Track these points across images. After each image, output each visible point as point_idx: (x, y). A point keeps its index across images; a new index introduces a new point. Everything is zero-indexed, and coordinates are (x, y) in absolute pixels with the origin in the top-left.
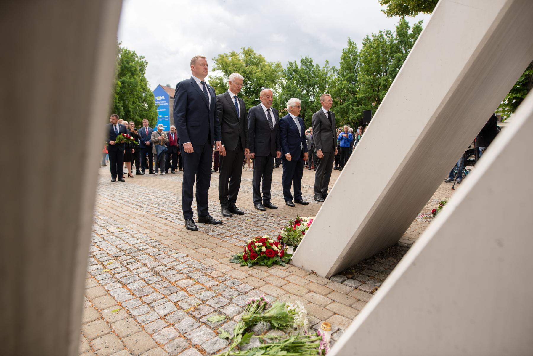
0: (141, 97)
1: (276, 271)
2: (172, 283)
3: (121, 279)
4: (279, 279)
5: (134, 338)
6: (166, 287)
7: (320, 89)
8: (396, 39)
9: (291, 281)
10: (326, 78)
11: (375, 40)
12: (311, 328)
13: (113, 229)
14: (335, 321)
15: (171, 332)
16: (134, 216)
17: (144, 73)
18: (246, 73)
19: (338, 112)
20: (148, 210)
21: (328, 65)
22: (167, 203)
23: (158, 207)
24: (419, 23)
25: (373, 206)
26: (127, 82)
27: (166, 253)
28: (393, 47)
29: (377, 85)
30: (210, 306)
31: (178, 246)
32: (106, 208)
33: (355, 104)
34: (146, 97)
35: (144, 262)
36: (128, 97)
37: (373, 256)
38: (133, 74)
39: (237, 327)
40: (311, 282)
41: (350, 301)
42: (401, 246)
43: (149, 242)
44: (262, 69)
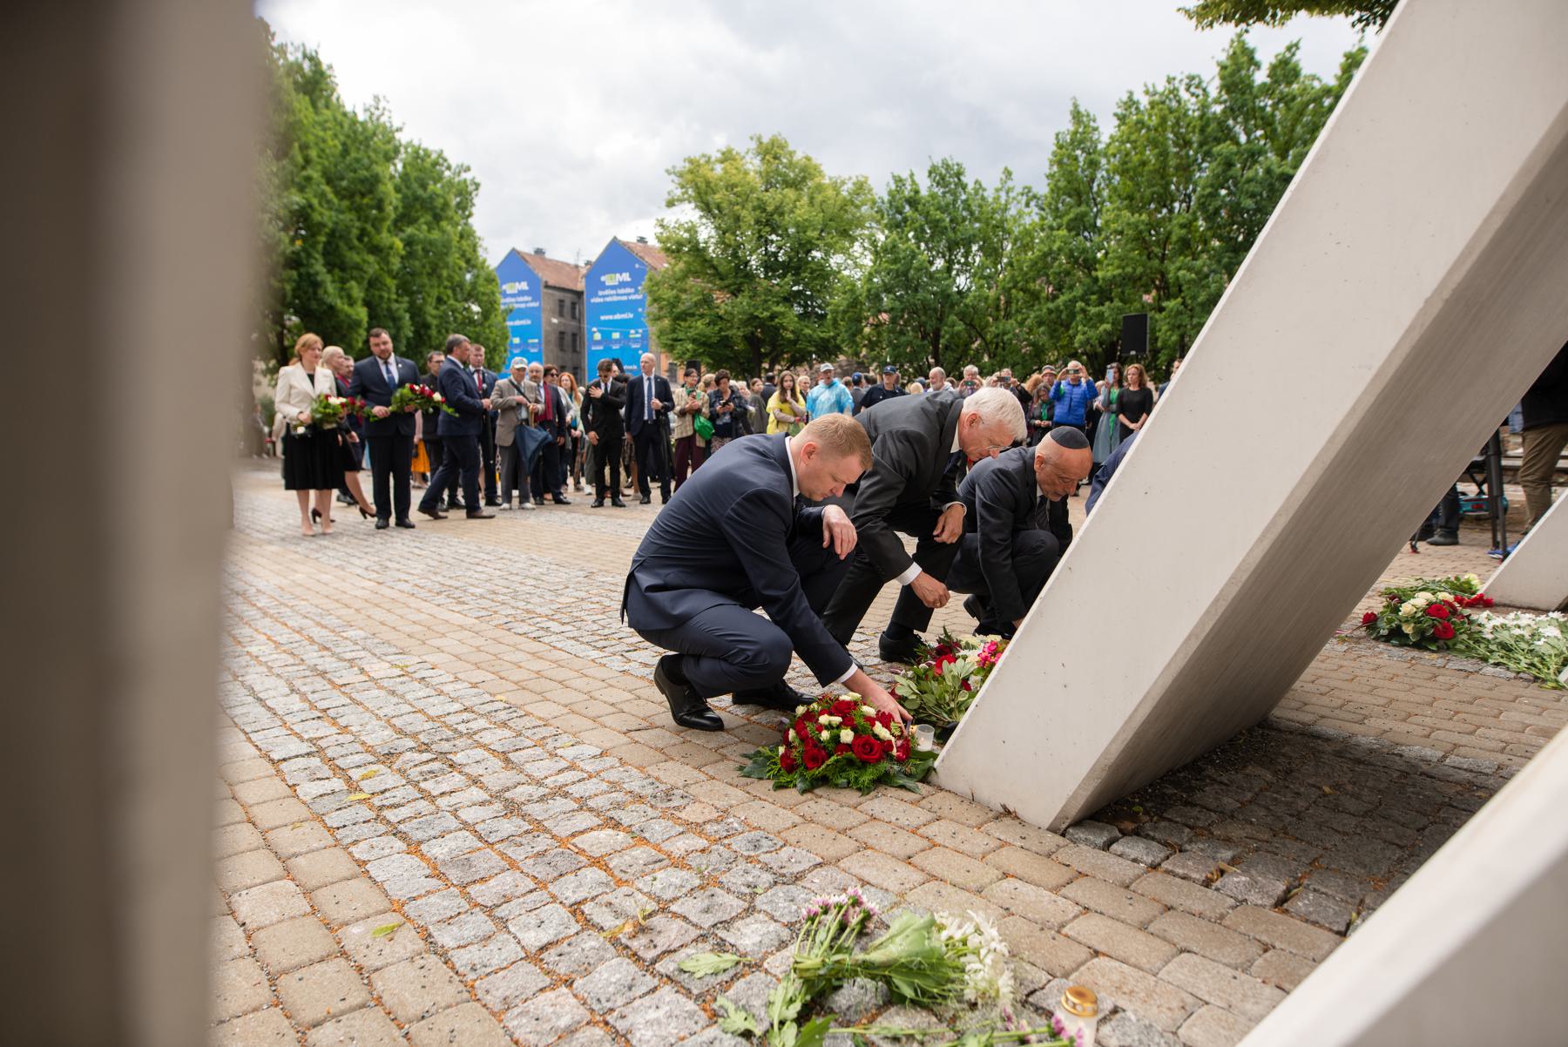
0: (461, 285)
1: (888, 804)
2: (561, 842)
3: (401, 827)
4: (899, 831)
5: (443, 1023)
6: (542, 854)
7: (987, 255)
8: (1217, 101)
9: (938, 840)
10: (1003, 221)
11: (1153, 105)
12: (1024, 1003)
13: (379, 669)
14: (1101, 981)
15: (562, 1008)
16: (441, 629)
17: (470, 215)
18: (764, 210)
19: (1040, 324)
20: (484, 613)
21: (1010, 184)
22: (538, 591)
23: (512, 602)
24: (1289, 49)
25: (1216, 600)
26: (421, 242)
28: (1207, 124)
29: (1158, 241)
30: (685, 918)
31: (576, 722)
32: (359, 604)
33: (1094, 297)
34: (474, 284)
35: (474, 770)
36: (424, 286)
37: (1194, 762)
38: (437, 218)
39: (779, 995)
40: (1004, 844)
41: (1140, 911)
42: (1279, 730)
43: (489, 707)
44: (812, 199)
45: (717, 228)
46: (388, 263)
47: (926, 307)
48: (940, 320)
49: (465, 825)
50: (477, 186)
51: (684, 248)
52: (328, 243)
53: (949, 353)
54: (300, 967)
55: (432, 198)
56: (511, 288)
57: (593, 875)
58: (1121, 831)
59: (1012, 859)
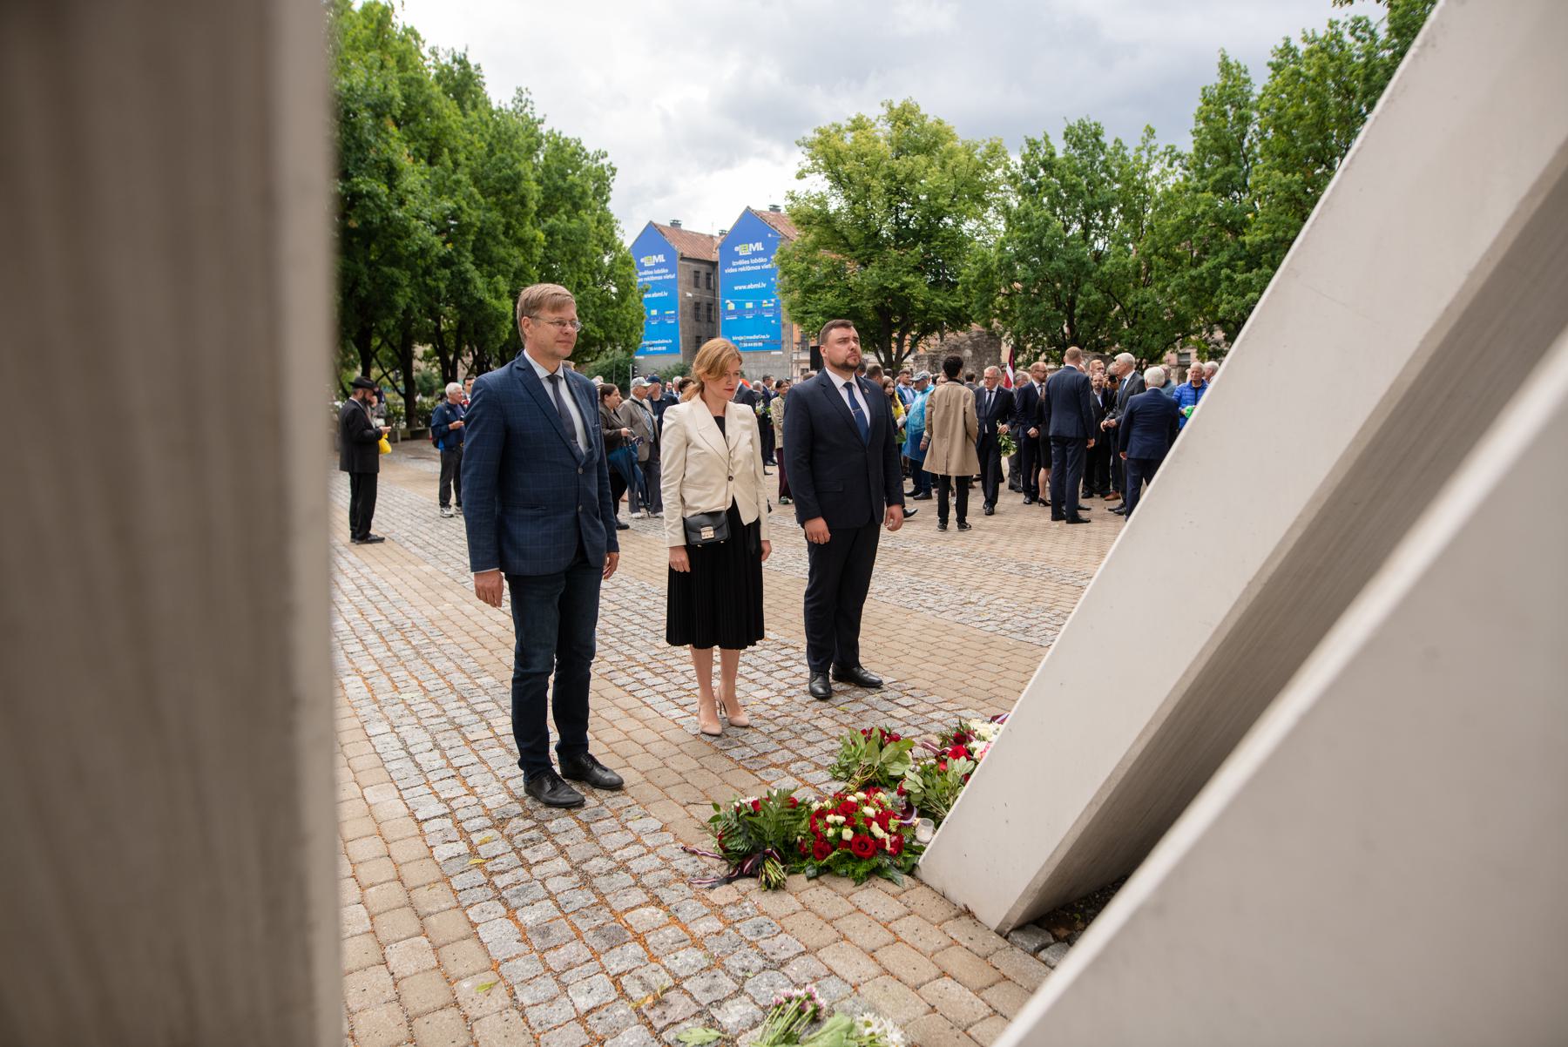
1: (875, 898)
8: (1385, 46)
9: (902, 936)
10: (1144, 181)
21: (1153, 142)
25: (1109, 779)
27: (616, 815)
28: (1373, 72)
32: (493, 644)
33: (1241, 263)
38: (576, 207)
44: (943, 165)
45: (848, 197)
46: (531, 255)
47: (1059, 276)
48: (1076, 288)
49: (550, 896)
50: (614, 171)
51: (816, 220)
52: (478, 239)
53: (1085, 323)
54: (427, 1013)
55: (573, 186)
56: (647, 261)
57: (633, 949)
58: (1055, 937)
59: (956, 960)
